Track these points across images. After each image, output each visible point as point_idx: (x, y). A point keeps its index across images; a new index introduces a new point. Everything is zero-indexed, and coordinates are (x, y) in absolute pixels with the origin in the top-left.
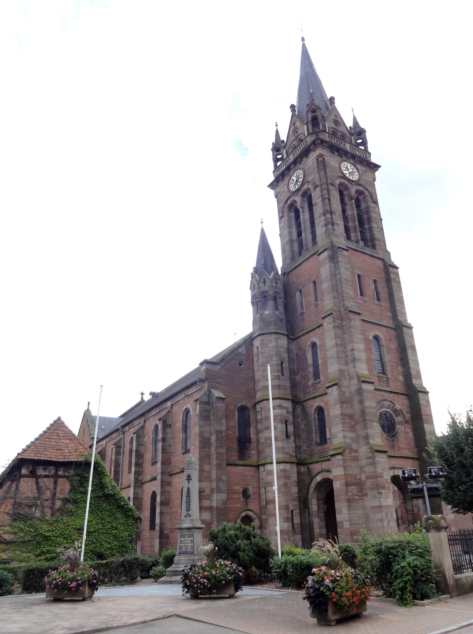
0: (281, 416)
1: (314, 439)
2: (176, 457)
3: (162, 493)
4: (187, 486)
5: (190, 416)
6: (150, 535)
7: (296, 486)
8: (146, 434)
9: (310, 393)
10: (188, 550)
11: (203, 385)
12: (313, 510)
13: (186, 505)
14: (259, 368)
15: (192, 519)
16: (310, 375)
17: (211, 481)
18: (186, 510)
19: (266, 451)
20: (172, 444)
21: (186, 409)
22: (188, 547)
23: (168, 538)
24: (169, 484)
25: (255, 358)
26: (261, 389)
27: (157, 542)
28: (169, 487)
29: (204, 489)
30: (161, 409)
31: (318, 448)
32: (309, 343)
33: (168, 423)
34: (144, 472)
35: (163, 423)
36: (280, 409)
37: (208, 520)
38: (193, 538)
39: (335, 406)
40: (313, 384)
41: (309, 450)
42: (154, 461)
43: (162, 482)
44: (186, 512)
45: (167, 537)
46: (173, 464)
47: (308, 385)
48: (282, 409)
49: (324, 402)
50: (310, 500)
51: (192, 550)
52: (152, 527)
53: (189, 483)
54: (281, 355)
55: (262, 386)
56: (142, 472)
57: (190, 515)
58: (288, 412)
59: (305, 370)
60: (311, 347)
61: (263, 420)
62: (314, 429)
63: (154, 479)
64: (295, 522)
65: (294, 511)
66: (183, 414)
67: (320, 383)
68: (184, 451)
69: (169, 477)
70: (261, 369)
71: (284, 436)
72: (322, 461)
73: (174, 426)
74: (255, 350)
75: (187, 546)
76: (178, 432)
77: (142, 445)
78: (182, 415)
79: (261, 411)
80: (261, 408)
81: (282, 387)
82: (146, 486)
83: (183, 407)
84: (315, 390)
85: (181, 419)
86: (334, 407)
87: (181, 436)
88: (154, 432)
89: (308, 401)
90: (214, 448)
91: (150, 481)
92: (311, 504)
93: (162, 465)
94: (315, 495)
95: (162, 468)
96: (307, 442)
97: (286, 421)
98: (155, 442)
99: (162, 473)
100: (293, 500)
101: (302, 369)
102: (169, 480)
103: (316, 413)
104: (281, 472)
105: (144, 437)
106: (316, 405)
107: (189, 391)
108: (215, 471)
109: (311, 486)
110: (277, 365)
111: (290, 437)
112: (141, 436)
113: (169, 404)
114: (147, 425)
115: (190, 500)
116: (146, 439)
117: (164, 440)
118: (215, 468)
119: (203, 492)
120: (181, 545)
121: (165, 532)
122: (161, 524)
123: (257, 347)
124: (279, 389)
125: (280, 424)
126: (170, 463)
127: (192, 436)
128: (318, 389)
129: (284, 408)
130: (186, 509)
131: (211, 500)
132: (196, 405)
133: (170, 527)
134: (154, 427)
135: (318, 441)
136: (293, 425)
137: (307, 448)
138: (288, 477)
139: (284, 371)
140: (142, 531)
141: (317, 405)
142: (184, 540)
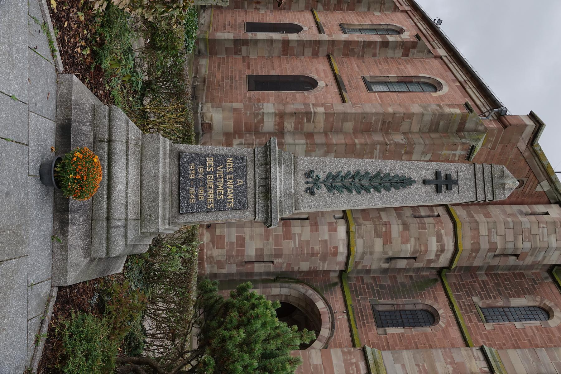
0: (426, 251)
1: (382, 301)
2: (357, 66)
3: (302, 44)
4: (415, 175)
5: (430, 92)
6: (239, 24)
7: (310, 268)
8: (385, 14)
9: (458, 297)
10: (193, 191)
11: (491, 118)
12: (273, 289)
13: (349, 173)
14: (509, 215)
15: (301, 199)
16: (490, 301)
17: (326, 134)
18: (329, 176)
19: (367, 223)
20: (376, 58)
21: (440, 84)
22: (201, 191)
23: (236, 53)
24: (315, 54)
25: (526, 208)
26: (473, 217)
27: (229, 35)
28: (310, 54)
29: (313, 122)
30: (430, 39)
31: (368, 308)
32: (548, 303)
33: (412, 51)
34: (327, 12)
35: (413, 42)
36: (437, 250)
37: (262, 126)
38: (231, 209)
39: (451, 363)
40: (474, 304)
41: (364, 288)
42: (346, 27)
43: (318, 43)
44: (323, 176)
45: (237, 52)
46: (345, 60)
47: (472, 295)
48: (437, 252)
49: (446, 326)
50: (287, 285)
51: (192, 206)
52: (253, 27)
53: (425, 182)
54: (532, 255)
55: (478, 220)
56: (328, 9)
57: (312, 193)
58: (430, 261)
59: (498, 290)
60: (542, 305)
61: (418, 219)
62: (399, 301)
63: (320, 30)
64: (256, 265)
65: (272, 265)
66: (429, 78)
67: (479, 321)
68: (368, 79)
69: (326, 54)
70: (509, 219)
71: (390, 254)
72: (348, 313)
73: (406, 61)
74: (541, 208)
75: (205, 186)
76: (398, 68)
77: (369, 9)
78: (427, 76)
79: (433, 216)
80: (438, 216)
81: (474, 254)
82: (308, 16)
83: (443, 78)
84: (466, 310)
85: (420, 75)
86: (449, 360)
87: (393, 73)
88: (389, 27)
89: (443, 293)
90: (382, 139)
91: (317, 23)
92: (281, 287)
93: (345, 41)
94: (294, 293)
95: (339, 42)
96: (376, 284)
97: (415, 258)
98: (375, 30)
99: (333, 43)
100: (289, 264)
101: (498, 285)
102: (320, 54)
103: (425, 307)
104: (334, 248)
105: (380, 11)
106: (440, 309)
107: (474, 89)
108: (343, 141)
109: (307, 288)
110: (516, 249)
111: (388, 262)
112: (383, 6)
113: (442, 52)
114: (399, 15)
115: (367, 190)
116: (377, 14)
117: (385, 44)
118: (349, 141)
119: (309, 120)
120: (210, 161)
121: (244, 49)
122: (256, 42)
123: (547, 214)
124: (472, 251)
125: (412, 250)
126: (346, 55)
127: (395, 94)
128: (469, 316)
129: (438, 256)
130: (334, 173)
131: (294, 134)
132: (458, 106)
133: (251, 56)
134: (398, 27)
135: (380, 308)
136: (408, 267)
137: (367, 284)
138: (324, 258)
139: (502, 258)
140: (246, 10)
141: (440, 312)
142: (225, 174)
